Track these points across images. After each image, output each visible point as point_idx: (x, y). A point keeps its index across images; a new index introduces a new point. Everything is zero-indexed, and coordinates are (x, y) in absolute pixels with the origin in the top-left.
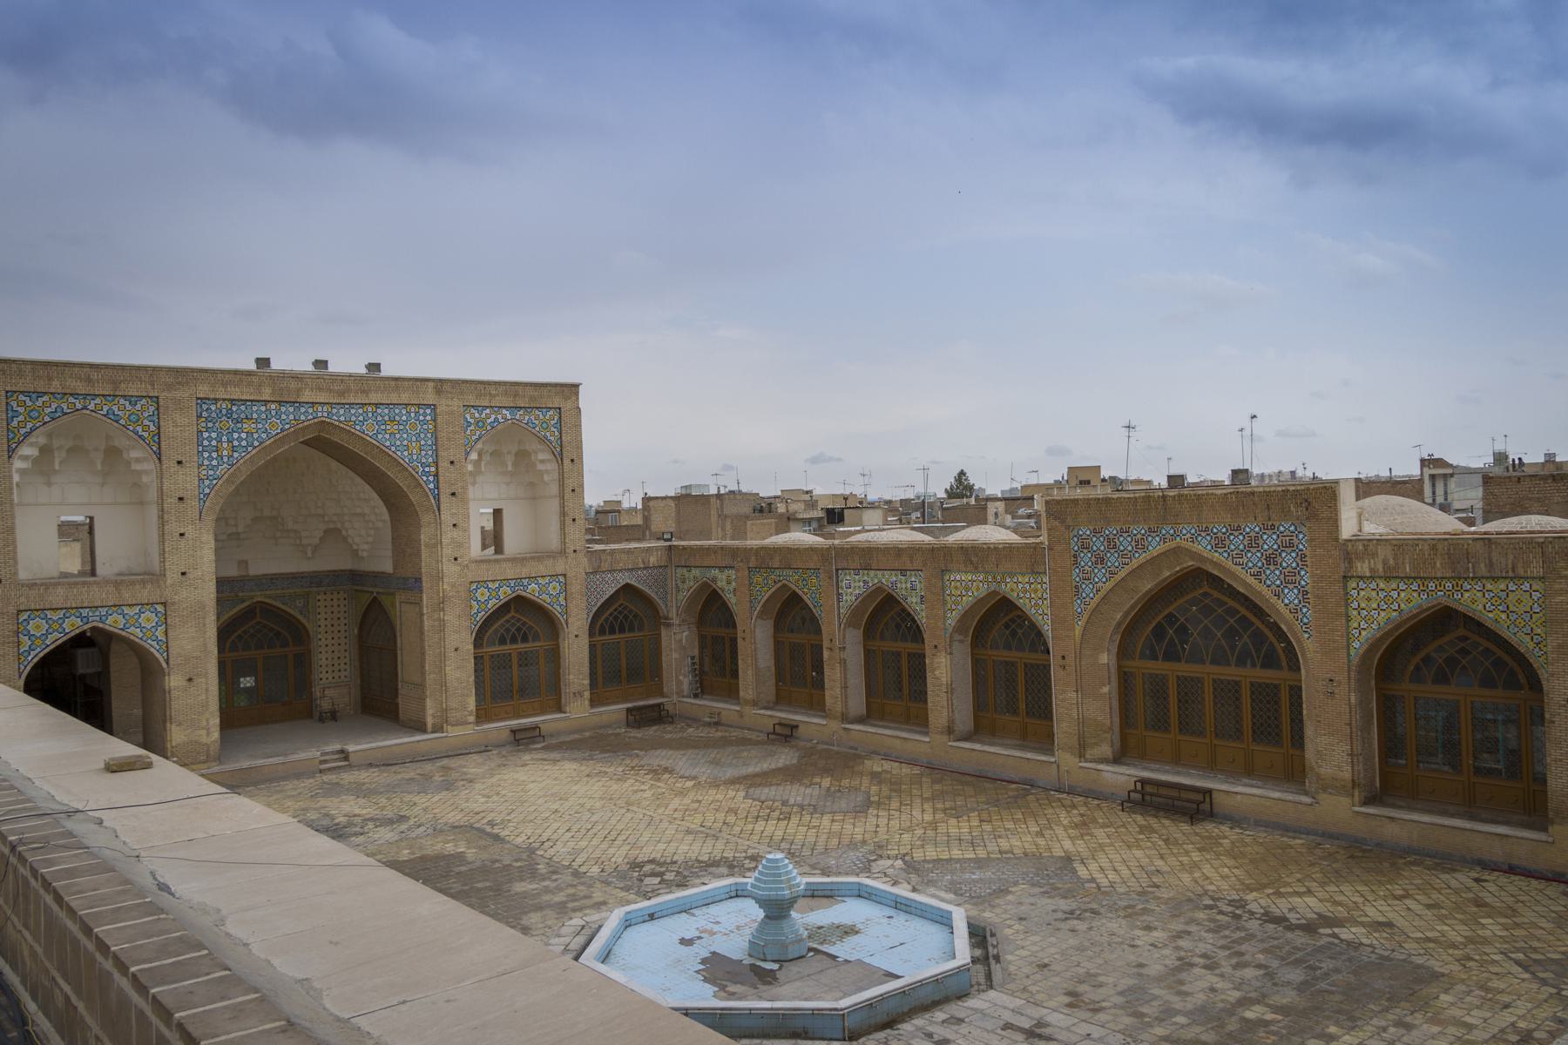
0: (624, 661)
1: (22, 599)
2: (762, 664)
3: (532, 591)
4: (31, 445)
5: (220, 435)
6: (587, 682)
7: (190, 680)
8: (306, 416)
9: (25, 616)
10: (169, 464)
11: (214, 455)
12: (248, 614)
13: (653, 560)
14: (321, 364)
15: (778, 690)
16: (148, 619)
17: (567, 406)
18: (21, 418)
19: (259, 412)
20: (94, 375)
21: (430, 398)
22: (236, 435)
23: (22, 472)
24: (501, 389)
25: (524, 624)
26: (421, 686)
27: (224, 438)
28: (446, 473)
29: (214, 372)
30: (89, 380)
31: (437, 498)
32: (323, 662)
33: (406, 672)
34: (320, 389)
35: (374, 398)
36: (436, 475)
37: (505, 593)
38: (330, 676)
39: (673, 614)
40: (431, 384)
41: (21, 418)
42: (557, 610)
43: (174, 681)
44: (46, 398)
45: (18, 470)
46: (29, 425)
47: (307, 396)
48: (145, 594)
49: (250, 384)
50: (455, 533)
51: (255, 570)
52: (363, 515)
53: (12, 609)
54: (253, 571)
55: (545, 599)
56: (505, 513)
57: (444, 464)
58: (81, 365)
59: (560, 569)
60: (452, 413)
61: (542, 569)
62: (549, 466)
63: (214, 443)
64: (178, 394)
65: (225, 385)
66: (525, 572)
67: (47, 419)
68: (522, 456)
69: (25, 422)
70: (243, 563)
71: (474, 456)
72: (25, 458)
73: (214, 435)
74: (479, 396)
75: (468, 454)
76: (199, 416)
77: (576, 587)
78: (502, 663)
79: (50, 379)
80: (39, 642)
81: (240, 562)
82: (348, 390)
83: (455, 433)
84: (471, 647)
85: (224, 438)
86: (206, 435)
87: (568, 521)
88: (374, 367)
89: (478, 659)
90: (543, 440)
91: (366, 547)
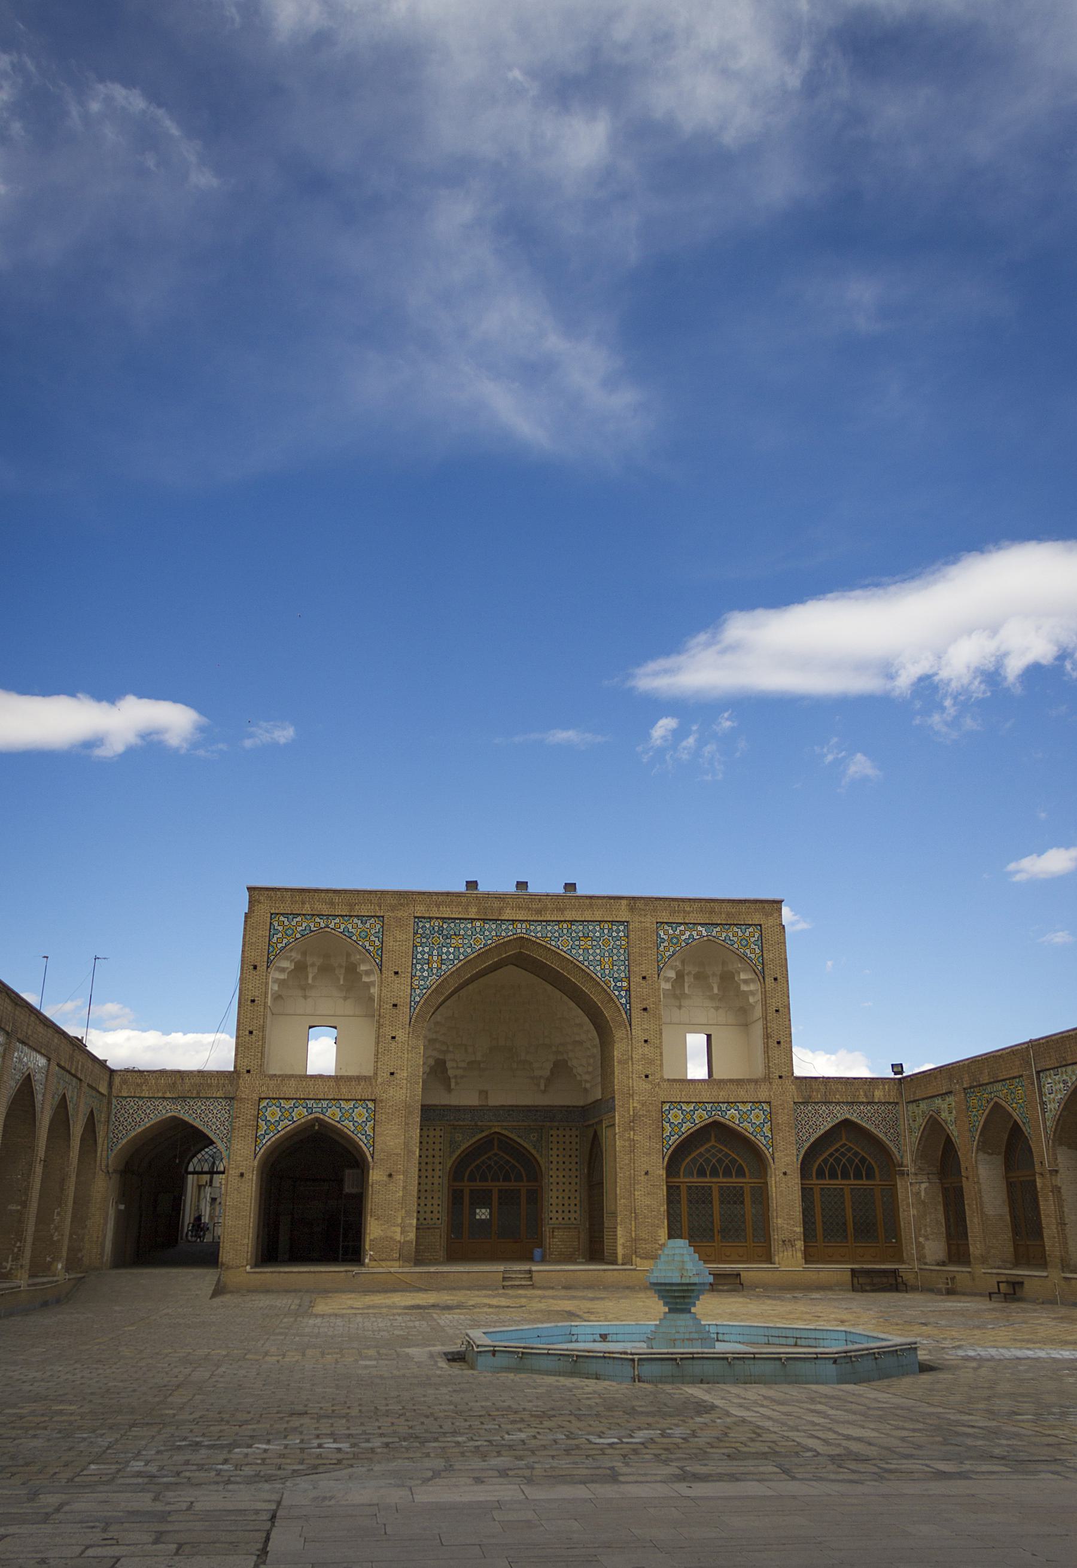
0: (849, 1212)
1: (264, 1088)
2: (989, 1210)
3: (731, 1116)
4: (287, 958)
5: (432, 949)
6: (799, 1229)
7: (390, 1175)
8: (508, 932)
9: (264, 1103)
10: (388, 974)
11: (426, 967)
12: (485, 1145)
13: (878, 1095)
14: (522, 885)
15: (1016, 1247)
16: (360, 1114)
17: (768, 923)
18: (280, 935)
19: (466, 929)
20: (336, 899)
21: (624, 915)
22: (445, 950)
23: (282, 983)
24: (696, 905)
25: (727, 1155)
26: (614, 1214)
27: (435, 952)
28: (639, 989)
29: (430, 894)
30: (332, 904)
31: (629, 1013)
32: (554, 1201)
33: (608, 1206)
34: (520, 908)
35: (569, 915)
36: (628, 990)
37: (701, 1117)
38: (560, 1216)
39: (908, 1160)
40: (624, 902)
41: (280, 935)
42: (761, 1141)
43: (376, 1176)
44: (299, 919)
45: (275, 981)
46: (285, 941)
47: (508, 914)
48: (359, 1091)
49: (459, 904)
50: (647, 1049)
51: (495, 1100)
52: (581, 1043)
53: (256, 1097)
55: (746, 1128)
56: (713, 1037)
57: (636, 979)
58: (327, 891)
59: (763, 1095)
60: (645, 929)
61: (742, 1094)
62: (752, 987)
63: (426, 956)
64: (400, 914)
65: (438, 906)
66: (722, 1095)
67: (298, 936)
68: (728, 979)
69: (282, 938)
71: (672, 974)
72: (283, 970)
73: (426, 949)
74: (673, 912)
75: (660, 970)
76: (416, 933)
77: (782, 1118)
78: (700, 1197)
79: (303, 903)
80: (272, 1128)
81: (481, 1092)
82: (545, 909)
83: (646, 948)
84: (663, 1173)
85: (435, 952)
86: (420, 949)
87: (772, 1043)
88: (570, 887)
89: (672, 1191)
90: (743, 958)
91: (587, 1077)
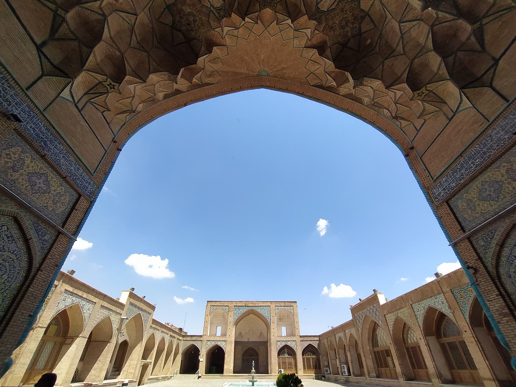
8: (250, 308)
37: (284, 344)
54: (250, 340)
70: (248, 339)
